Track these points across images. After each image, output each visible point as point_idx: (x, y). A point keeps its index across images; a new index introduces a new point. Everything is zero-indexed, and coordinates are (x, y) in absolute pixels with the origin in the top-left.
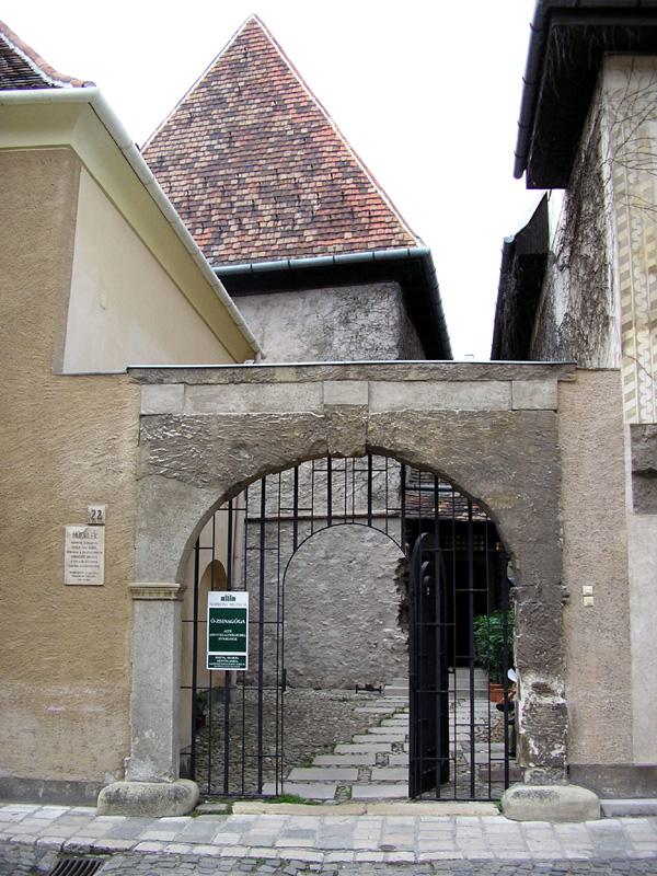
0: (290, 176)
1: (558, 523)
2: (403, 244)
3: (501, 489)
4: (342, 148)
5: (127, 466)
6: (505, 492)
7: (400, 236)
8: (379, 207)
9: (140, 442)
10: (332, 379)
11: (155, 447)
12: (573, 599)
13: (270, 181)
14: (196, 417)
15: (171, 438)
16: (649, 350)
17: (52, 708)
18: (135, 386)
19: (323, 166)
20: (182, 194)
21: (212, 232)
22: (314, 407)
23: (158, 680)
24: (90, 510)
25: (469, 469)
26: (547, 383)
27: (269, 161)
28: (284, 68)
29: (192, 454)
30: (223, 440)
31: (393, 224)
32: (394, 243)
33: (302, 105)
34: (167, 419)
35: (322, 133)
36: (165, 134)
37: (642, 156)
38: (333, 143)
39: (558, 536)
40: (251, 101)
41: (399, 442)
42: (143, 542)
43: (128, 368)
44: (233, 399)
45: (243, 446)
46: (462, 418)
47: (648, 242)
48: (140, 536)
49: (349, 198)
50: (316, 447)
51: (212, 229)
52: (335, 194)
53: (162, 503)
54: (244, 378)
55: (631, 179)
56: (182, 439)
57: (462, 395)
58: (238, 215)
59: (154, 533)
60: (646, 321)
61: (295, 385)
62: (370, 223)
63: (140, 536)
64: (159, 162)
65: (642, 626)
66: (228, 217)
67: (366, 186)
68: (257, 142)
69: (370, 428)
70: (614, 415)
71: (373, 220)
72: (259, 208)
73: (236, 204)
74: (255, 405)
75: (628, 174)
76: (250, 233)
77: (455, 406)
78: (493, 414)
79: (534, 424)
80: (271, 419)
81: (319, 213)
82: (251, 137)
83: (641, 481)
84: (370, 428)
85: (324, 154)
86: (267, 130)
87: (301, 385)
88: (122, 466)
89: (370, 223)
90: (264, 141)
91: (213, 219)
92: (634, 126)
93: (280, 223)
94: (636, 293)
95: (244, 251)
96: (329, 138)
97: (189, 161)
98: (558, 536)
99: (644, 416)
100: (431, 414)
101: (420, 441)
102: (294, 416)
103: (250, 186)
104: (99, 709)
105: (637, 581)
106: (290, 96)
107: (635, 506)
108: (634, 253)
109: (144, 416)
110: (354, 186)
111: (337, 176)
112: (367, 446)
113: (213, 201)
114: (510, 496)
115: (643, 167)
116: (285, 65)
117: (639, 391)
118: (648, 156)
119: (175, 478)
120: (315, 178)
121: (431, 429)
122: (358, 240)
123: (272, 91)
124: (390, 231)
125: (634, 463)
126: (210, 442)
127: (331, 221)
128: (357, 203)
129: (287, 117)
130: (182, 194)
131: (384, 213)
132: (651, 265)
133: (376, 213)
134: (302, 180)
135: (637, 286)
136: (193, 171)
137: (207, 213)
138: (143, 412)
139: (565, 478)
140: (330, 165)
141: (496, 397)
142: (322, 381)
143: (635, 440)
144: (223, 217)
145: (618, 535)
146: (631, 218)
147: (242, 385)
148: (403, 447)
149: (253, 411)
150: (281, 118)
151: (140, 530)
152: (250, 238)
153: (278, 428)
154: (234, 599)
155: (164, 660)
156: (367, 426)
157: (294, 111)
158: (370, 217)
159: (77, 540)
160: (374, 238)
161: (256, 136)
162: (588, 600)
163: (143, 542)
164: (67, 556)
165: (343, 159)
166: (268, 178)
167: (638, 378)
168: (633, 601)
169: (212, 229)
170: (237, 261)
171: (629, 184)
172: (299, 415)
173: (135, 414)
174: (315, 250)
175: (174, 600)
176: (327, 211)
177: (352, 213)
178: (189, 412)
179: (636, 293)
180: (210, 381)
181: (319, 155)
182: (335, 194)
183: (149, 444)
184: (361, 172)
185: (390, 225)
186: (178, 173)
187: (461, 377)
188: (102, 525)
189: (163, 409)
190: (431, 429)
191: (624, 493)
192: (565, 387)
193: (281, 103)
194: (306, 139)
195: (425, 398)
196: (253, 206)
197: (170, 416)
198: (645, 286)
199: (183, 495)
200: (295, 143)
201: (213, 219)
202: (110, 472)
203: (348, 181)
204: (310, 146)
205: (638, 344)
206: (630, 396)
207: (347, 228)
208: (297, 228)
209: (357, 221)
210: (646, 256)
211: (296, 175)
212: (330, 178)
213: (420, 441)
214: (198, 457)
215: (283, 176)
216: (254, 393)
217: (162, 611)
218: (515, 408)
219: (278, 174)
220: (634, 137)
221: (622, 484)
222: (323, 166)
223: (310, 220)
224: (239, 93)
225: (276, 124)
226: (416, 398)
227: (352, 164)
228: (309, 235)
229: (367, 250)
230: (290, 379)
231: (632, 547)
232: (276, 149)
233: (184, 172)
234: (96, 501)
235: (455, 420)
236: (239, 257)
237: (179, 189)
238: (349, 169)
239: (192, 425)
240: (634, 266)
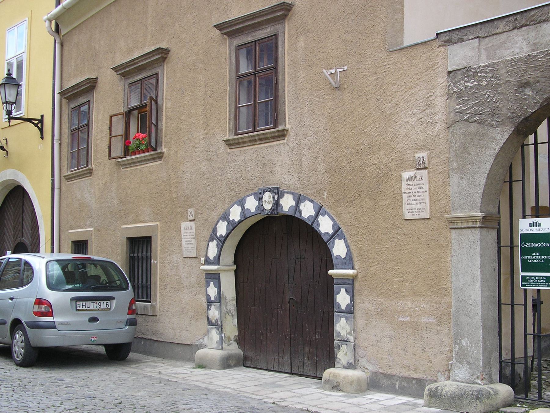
9: (449, 96)
17: (401, 319)
24: (416, 158)
42: (455, 179)
44: (517, 43)
45: (526, 84)
54: (524, 22)
56: (479, 87)
74: (535, 44)
88: (437, 118)
104: (432, 320)
126: (500, 85)
138: (450, 69)
147: (523, 28)
149: (533, 50)
151: (453, 169)
154: (540, 225)
159: (410, 183)
163: (455, 179)
164: (404, 196)
216: (533, 34)
217: (471, 238)
234: (421, 149)
239: (486, 73)
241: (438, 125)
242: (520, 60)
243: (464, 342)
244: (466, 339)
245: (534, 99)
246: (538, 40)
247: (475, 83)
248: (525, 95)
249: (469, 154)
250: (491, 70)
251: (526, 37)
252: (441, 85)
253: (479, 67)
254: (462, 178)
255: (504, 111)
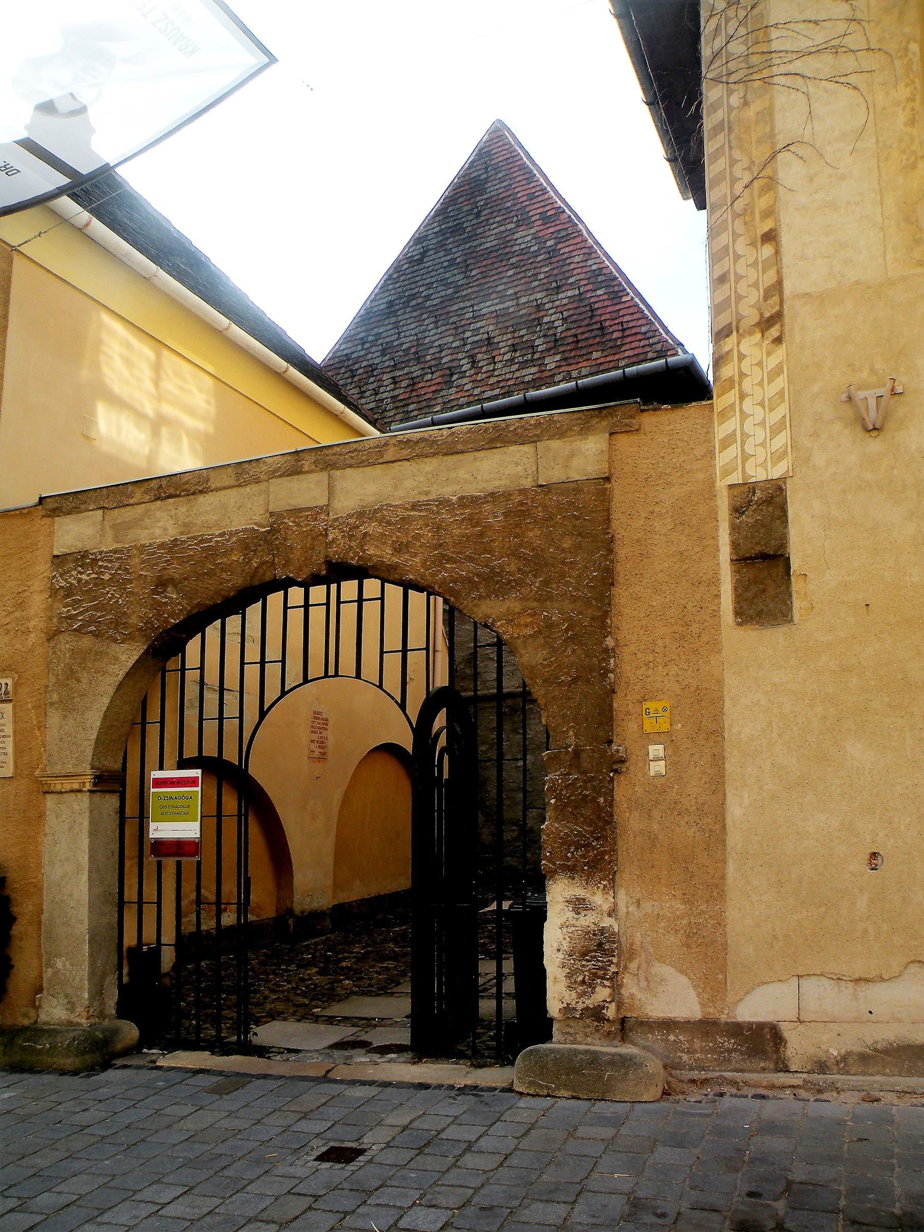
0: (532, 298)
1: (606, 650)
2: (661, 354)
3: (517, 606)
4: (593, 256)
5: (37, 622)
6: (524, 610)
7: (658, 347)
8: (635, 316)
9: (54, 592)
10: (280, 476)
11: (68, 596)
12: (632, 767)
13: (508, 308)
14: (115, 552)
15: (87, 582)
16: (760, 364)
18: (47, 521)
19: (571, 280)
20: (412, 338)
21: (443, 376)
22: (258, 518)
23: (71, 895)
25: (470, 581)
26: (592, 439)
27: (510, 285)
28: (529, 176)
29: (110, 598)
30: (146, 576)
31: (651, 334)
32: (650, 355)
33: (549, 214)
34: (82, 558)
35: (571, 242)
36: (395, 276)
37: (754, 59)
38: (583, 251)
39: (607, 671)
40: (492, 221)
41: (371, 552)
42: (54, 719)
43: (41, 499)
44: (159, 521)
45: (171, 581)
46: (464, 506)
47: (760, 196)
48: (51, 712)
49: (599, 312)
50: (261, 571)
51: (442, 373)
52: (583, 309)
53: (75, 667)
55: (735, 100)
56: (99, 582)
57: (462, 474)
58: (472, 352)
59: (67, 706)
60: (757, 319)
61: (235, 490)
62: (623, 337)
63: (51, 712)
64: (387, 308)
65: (746, 802)
66: (460, 356)
67: (620, 294)
68: (496, 266)
69: (330, 537)
70: (700, 476)
71: (626, 333)
72: (495, 340)
73: (470, 340)
74: (185, 525)
75: (730, 93)
76: (484, 369)
77: (450, 491)
78: (507, 495)
79: (570, 503)
80: (202, 541)
81: (563, 335)
82: (490, 262)
83: (749, 573)
84: (330, 537)
85: (572, 266)
86: (507, 250)
87: (242, 490)
88: (31, 625)
89: (623, 337)
90: (504, 263)
91: (444, 360)
92: (742, 14)
93: (518, 354)
94: (739, 278)
95: (476, 391)
96: (579, 246)
97: (420, 300)
98: (607, 671)
99: (750, 471)
100: (415, 506)
101: (399, 549)
102: (231, 534)
103: (487, 316)
105: (739, 733)
106: (536, 206)
107: (738, 613)
108: (736, 216)
109: (57, 556)
110: (606, 297)
111: (587, 288)
112: (329, 564)
113: (445, 341)
114: (531, 615)
115: (755, 77)
116: (531, 172)
117: (743, 433)
118: (765, 57)
119: (90, 632)
120: (560, 296)
121: (416, 528)
122: (608, 359)
123: (515, 205)
124: (646, 342)
125: (735, 545)
126: (130, 581)
127: (578, 342)
128: (608, 316)
129: (532, 231)
130: (412, 338)
131: (640, 322)
132: (766, 229)
133: (631, 325)
134: (545, 300)
135: (741, 268)
136: (424, 311)
137: (438, 355)
138: (56, 553)
139: (621, 579)
140: (579, 277)
141: (512, 470)
142: (267, 481)
143: (737, 511)
144: (454, 356)
145: (708, 662)
146: (733, 162)
148: (375, 559)
149: (182, 533)
150: (524, 233)
151: (52, 704)
152: (484, 376)
153: (212, 552)
155: (78, 871)
156: (327, 535)
157: (540, 222)
158: (623, 330)
160: (627, 354)
161: (494, 260)
162: (658, 768)
163: (54, 719)
165: (594, 267)
166: (506, 305)
167: (741, 411)
168: (731, 766)
169: (442, 373)
170: (469, 404)
171: (730, 109)
172: (237, 532)
173: (48, 557)
174: (556, 379)
175: (90, 791)
176: (573, 332)
177: (602, 328)
178: (108, 545)
179: (739, 278)
180: (131, 501)
181: (566, 268)
182: (583, 309)
183: (62, 593)
184: (615, 278)
185: (648, 335)
186: (407, 316)
187: (460, 447)
188: (10, 701)
189: (79, 546)
190: (416, 528)
191: (718, 596)
192: (623, 440)
193: (524, 216)
194: (552, 253)
195: (409, 484)
196: (489, 339)
197: (84, 554)
198: (755, 264)
199: (100, 655)
200: (540, 258)
201: (444, 360)
202: (19, 633)
203: (599, 292)
204: (556, 259)
205: (741, 357)
206: (727, 442)
207: (596, 347)
208: (536, 356)
209: (608, 337)
210: (757, 216)
211: (539, 296)
212: (577, 292)
213: (399, 549)
214: (117, 602)
215: (523, 300)
216: (184, 509)
218: (542, 482)
219: (518, 298)
220: (742, 31)
221: (715, 581)
222: (571, 280)
223: (553, 344)
224: (478, 215)
225: (518, 242)
226: (396, 487)
227: (604, 271)
228: (551, 362)
229: (616, 368)
230: (227, 483)
231: (731, 681)
232: (518, 270)
233: (415, 314)
235: (451, 511)
236: (471, 399)
237: (408, 333)
238: (600, 279)
239: (110, 561)
240: (736, 236)
241: (33, 635)
242: (162, 546)
243: (59, 965)
244: (64, 959)
245: (179, 604)
246: (190, 519)
247: (93, 576)
248: (166, 597)
249: (79, 681)
250: (118, 559)
251: (173, 513)
252: (42, 576)
253: (101, 553)
254: (65, 716)
255: (134, 620)
